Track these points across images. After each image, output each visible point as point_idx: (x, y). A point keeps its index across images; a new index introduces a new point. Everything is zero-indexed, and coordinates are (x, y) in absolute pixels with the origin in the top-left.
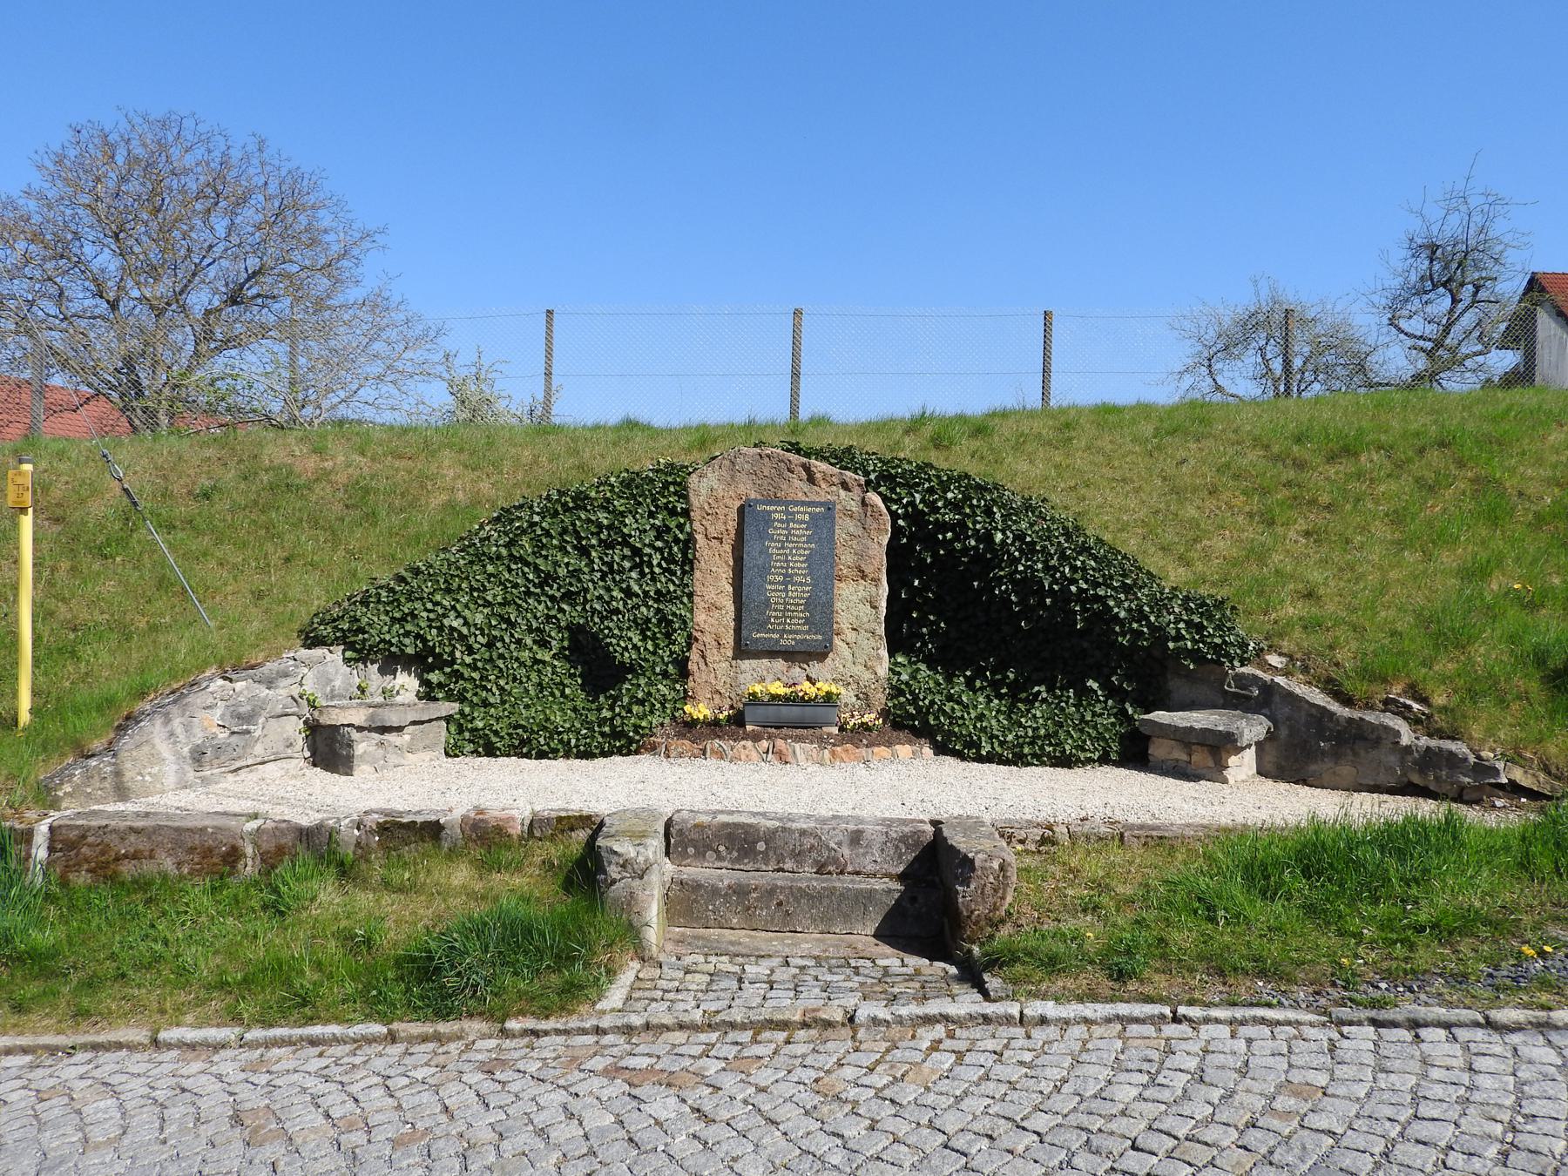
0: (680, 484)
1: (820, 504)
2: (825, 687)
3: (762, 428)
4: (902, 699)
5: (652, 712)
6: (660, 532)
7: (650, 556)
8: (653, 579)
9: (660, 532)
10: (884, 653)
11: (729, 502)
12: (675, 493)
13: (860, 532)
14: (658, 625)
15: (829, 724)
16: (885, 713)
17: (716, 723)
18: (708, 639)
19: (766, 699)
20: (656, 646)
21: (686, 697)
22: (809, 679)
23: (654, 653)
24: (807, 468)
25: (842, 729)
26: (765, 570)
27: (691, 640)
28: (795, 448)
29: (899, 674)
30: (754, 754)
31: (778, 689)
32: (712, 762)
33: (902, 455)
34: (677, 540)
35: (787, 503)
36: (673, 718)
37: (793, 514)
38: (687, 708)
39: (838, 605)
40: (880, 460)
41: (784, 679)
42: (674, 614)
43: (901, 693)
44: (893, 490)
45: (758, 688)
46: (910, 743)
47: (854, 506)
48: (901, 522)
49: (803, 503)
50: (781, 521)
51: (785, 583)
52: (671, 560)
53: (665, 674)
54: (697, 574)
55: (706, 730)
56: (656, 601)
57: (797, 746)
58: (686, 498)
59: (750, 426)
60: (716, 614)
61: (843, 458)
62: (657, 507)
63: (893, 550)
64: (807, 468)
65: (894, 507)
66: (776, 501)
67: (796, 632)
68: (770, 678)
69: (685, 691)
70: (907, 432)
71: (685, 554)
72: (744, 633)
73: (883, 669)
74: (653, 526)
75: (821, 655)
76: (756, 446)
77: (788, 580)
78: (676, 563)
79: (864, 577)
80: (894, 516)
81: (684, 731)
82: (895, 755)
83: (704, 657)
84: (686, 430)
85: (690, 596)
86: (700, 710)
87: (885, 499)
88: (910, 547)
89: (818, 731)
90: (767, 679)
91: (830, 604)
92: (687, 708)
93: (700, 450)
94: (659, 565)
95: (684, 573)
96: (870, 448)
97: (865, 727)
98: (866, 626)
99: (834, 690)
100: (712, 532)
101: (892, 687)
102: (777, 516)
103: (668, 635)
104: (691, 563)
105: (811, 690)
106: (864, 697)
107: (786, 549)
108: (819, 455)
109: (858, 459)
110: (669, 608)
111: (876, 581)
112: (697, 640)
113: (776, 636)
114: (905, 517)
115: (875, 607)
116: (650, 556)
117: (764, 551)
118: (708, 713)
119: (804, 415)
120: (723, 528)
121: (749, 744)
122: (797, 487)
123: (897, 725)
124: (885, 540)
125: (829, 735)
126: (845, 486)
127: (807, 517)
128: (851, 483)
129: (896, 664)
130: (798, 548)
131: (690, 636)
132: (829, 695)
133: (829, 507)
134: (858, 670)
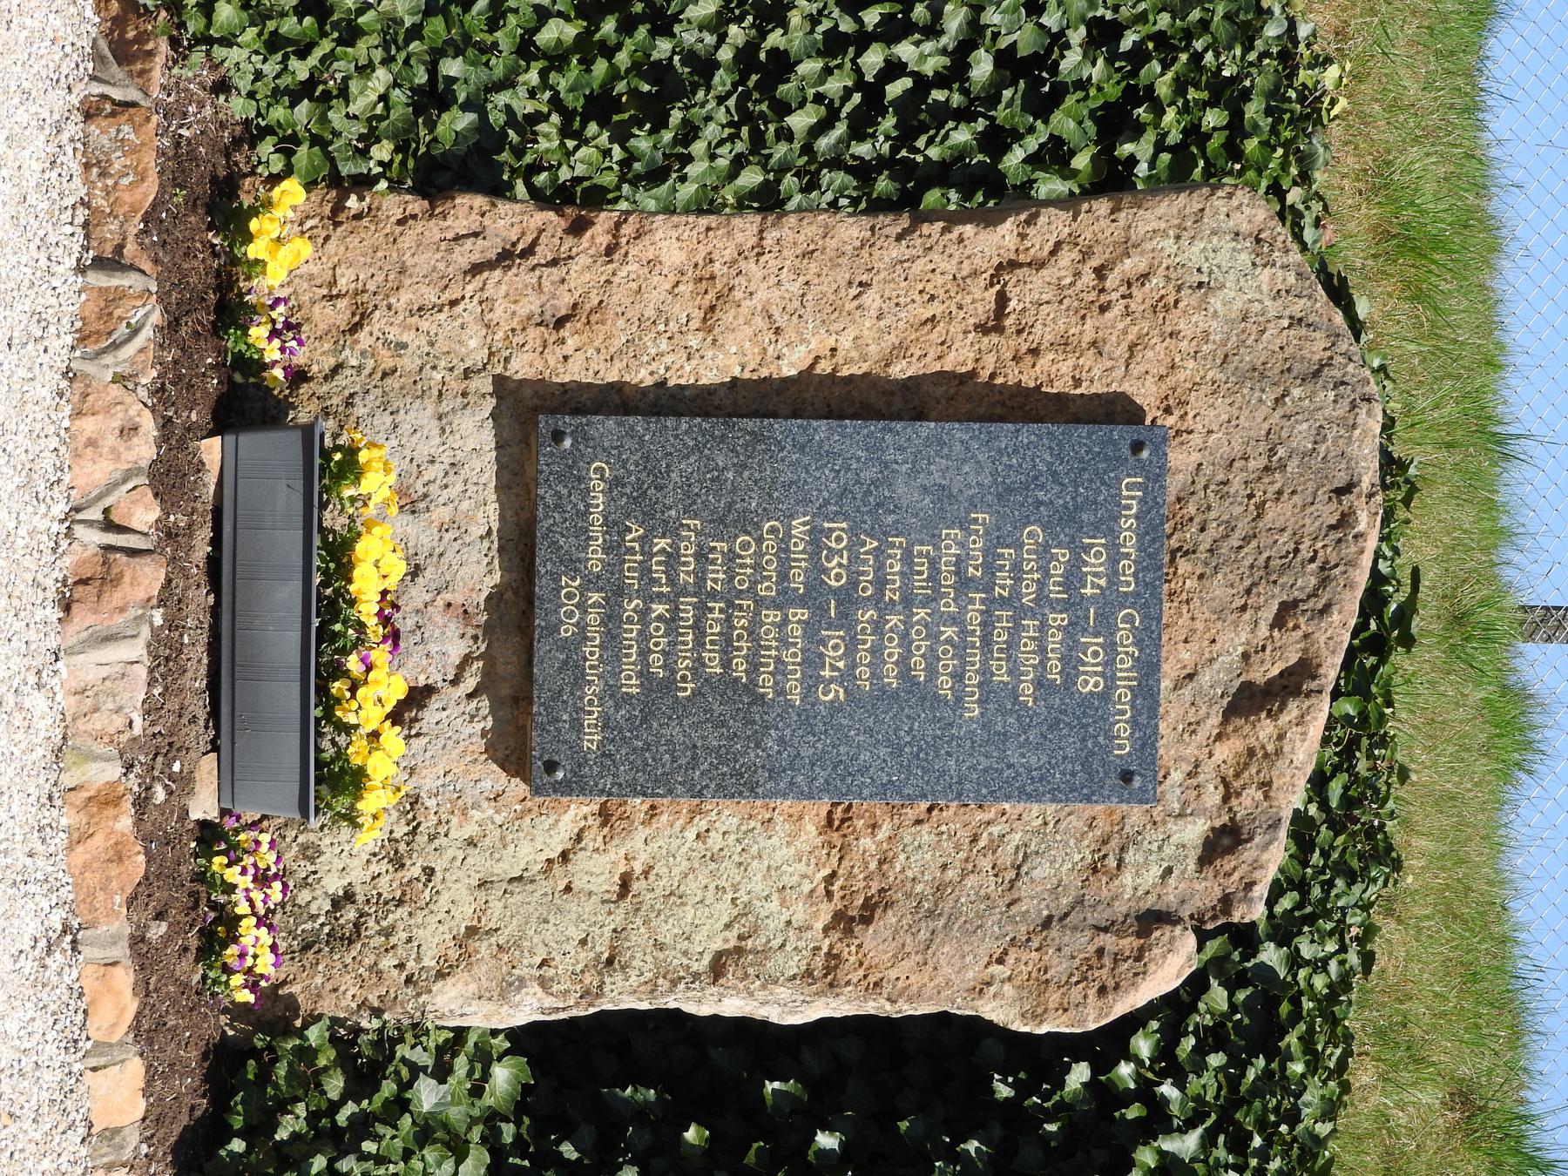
0: (1233, 150)
1: (1147, 741)
2: (384, 762)
3: (1480, 492)
4: (335, 1085)
5: (274, 43)
6: (1031, 73)
7: (933, 30)
8: (834, 44)
9: (1031, 73)
10: (527, 1009)
11: (1153, 358)
12: (1194, 133)
13: (1033, 904)
14: (645, 67)
15: (228, 780)
16: (275, 1013)
17: (231, 311)
18: (583, 275)
19: (333, 519)
20: (556, 59)
21: (338, 184)
22: (418, 697)
23: (526, 49)
24: (1297, 681)
25: (209, 835)
26: (871, 511)
27: (577, 202)
28: (1383, 629)
29: (442, 1072)
30: (97, 472)
31: (375, 569)
32: (67, 295)
33: (1363, 1075)
34: (997, 140)
35: (1149, 600)
36: (252, 134)
37: (1106, 626)
38: (291, 193)
39: (726, 816)
40: (1342, 985)
41: (417, 594)
42: (689, 132)
43: (363, 1080)
44: (1213, 1038)
45: (376, 484)
46: (154, 1119)
47: (1138, 882)
48: (1079, 1074)
49: (1149, 668)
50: (1073, 579)
51: (814, 596)
52: (917, 117)
53: (433, 98)
54: (851, 230)
55: (199, 270)
56: (746, 58)
57: (136, 650)
58: (1178, 177)
59: (1486, 440)
60: (686, 308)
61: (1347, 833)
62: (1138, 56)
63: (958, 1042)
64: (1297, 681)
65: (1143, 1045)
66: (1160, 556)
67: (612, 639)
68: (421, 532)
69: (363, 183)
70: (1464, 1098)
71: (941, 174)
72: (606, 427)
73: (461, 1004)
74: (1058, 40)
75: (514, 750)
76: (1390, 464)
77: (832, 606)
78: (905, 136)
79: (843, 923)
80: (1108, 1044)
81: (198, 177)
82: (101, 1056)
83: (506, 258)
84: (1472, 173)
85: (768, 201)
86: (282, 247)
87: (1174, 1009)
88: (976, 1112)
89: (198, 735)
90: (418, 522)
91: (740, 783)
92: (291, 193)
93: (1382, 233)
94: (894, 68)
95: (864, 172)
96: (1392, 941)
97: (217, 933)
98: (638, 937)
99: (372, 801)
100: (1026, 291)
101: (386, 1044)
102: (1095, 563)
103: (601, 106)
104: (906, 202)
105: (369, 707)
106: (344, 928)
107: (936, 588)
108: (1358, 737)
109: (1346, 895)
110: (714, 113)
111: (828, 974)
112: (578, 228)
113: (595, 558)
114: (1102, 1093)
115: (717, 969)
116: (933, 30)
117: (947, 507)
118: (274, 278)
119: (1544, 665)
120: (1043, 333)
121: (144, 449)
122: (1215, 641)
123: (226, 1065)
124: (1001, 1011)
125: (185, 783)
126: (1224, 842)
127: (1090, 684)
128: (1237, 864)
129: (483, 1058)
130: (961, 649)
131: (597, 198)
132: (349, 780)
133: (1133, 778)
134: (457, 901)
